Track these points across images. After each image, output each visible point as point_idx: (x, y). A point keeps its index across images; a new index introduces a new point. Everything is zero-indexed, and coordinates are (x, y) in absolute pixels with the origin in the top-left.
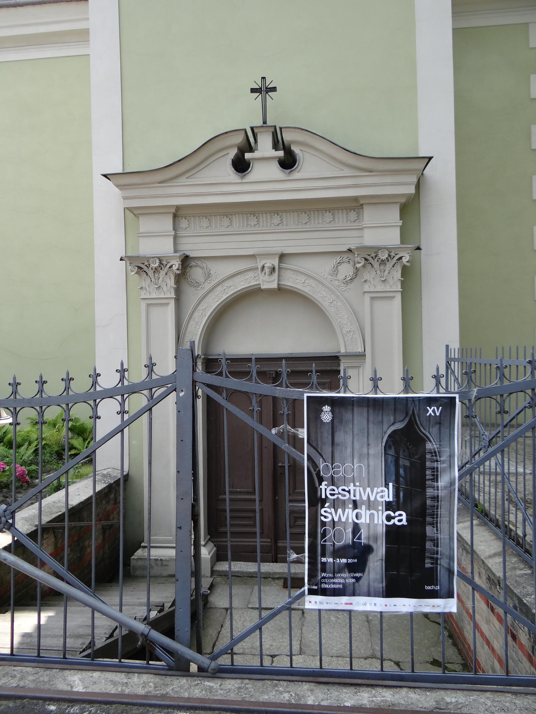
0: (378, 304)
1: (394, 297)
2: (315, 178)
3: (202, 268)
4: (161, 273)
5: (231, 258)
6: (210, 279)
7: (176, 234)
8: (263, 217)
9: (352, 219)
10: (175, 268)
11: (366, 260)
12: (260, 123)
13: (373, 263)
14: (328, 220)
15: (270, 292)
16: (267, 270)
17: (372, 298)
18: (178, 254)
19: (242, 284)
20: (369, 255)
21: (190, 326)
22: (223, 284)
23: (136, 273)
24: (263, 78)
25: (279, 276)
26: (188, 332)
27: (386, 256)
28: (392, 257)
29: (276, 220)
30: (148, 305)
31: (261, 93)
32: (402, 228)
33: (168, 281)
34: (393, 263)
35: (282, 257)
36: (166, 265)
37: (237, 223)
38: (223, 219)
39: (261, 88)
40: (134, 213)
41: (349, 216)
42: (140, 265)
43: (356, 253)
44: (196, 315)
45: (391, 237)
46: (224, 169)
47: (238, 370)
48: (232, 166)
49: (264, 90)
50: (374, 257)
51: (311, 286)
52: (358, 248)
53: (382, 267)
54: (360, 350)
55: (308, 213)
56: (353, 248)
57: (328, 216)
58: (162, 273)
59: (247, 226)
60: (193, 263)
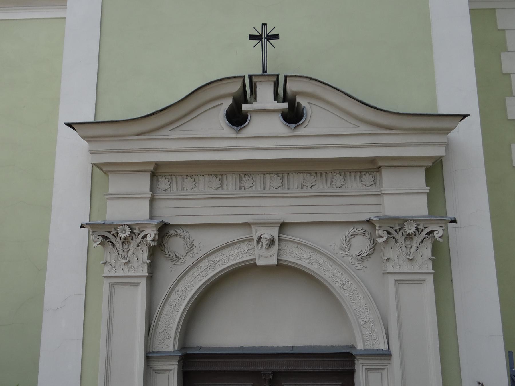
0: (404, 288)
2: (325, 134)
3: (183, 238)
4: (132, 245)
5: (220, 225)
6: (193, 251)
7: (153, 196)
8: (260, 179)
9: (368, 183)
10: (149, 238)
11: (389, 233)
12: (260, 72)
13: (397, 238)
14: (339, 184)
15: (267, 269)
16: (265, 243)
17: (397, 281)
18: (155, 222)
19: (232, 258)
20: (391, 227)
21: (164, 312)
22: (209, 258)
23: (100, 244)
24: (264, 25)
25: (279, 249)
26: (162, 319)
27: (414, 229)
28: (420, 230)
29: (276, 182)
30: (113, 285)
31: (261, 40)
32: (429, 196)
33: (140, 255)
34: (422, 238)
35: (283, 226)
36: (423, 230)
37: (229, 185)
38: (211, 180)
39: (261, 35)
40: (103, 170)
41: (363, 180)
42: (105, 234)
43: (377, 226)
44: (173, 297)
45: (417, 206)
46: (216, 120)
47: (225, 369)
48: (225, 118)
49: (264, 37)
50: (398, 231)
51: (318, 262)
53: (408, 243)
54: (383, 346)
55: (315, 174)
56: (375, 219)
57: (339, 180)
58: (133, 244)
59: (241, 189)
60: (172, 232)
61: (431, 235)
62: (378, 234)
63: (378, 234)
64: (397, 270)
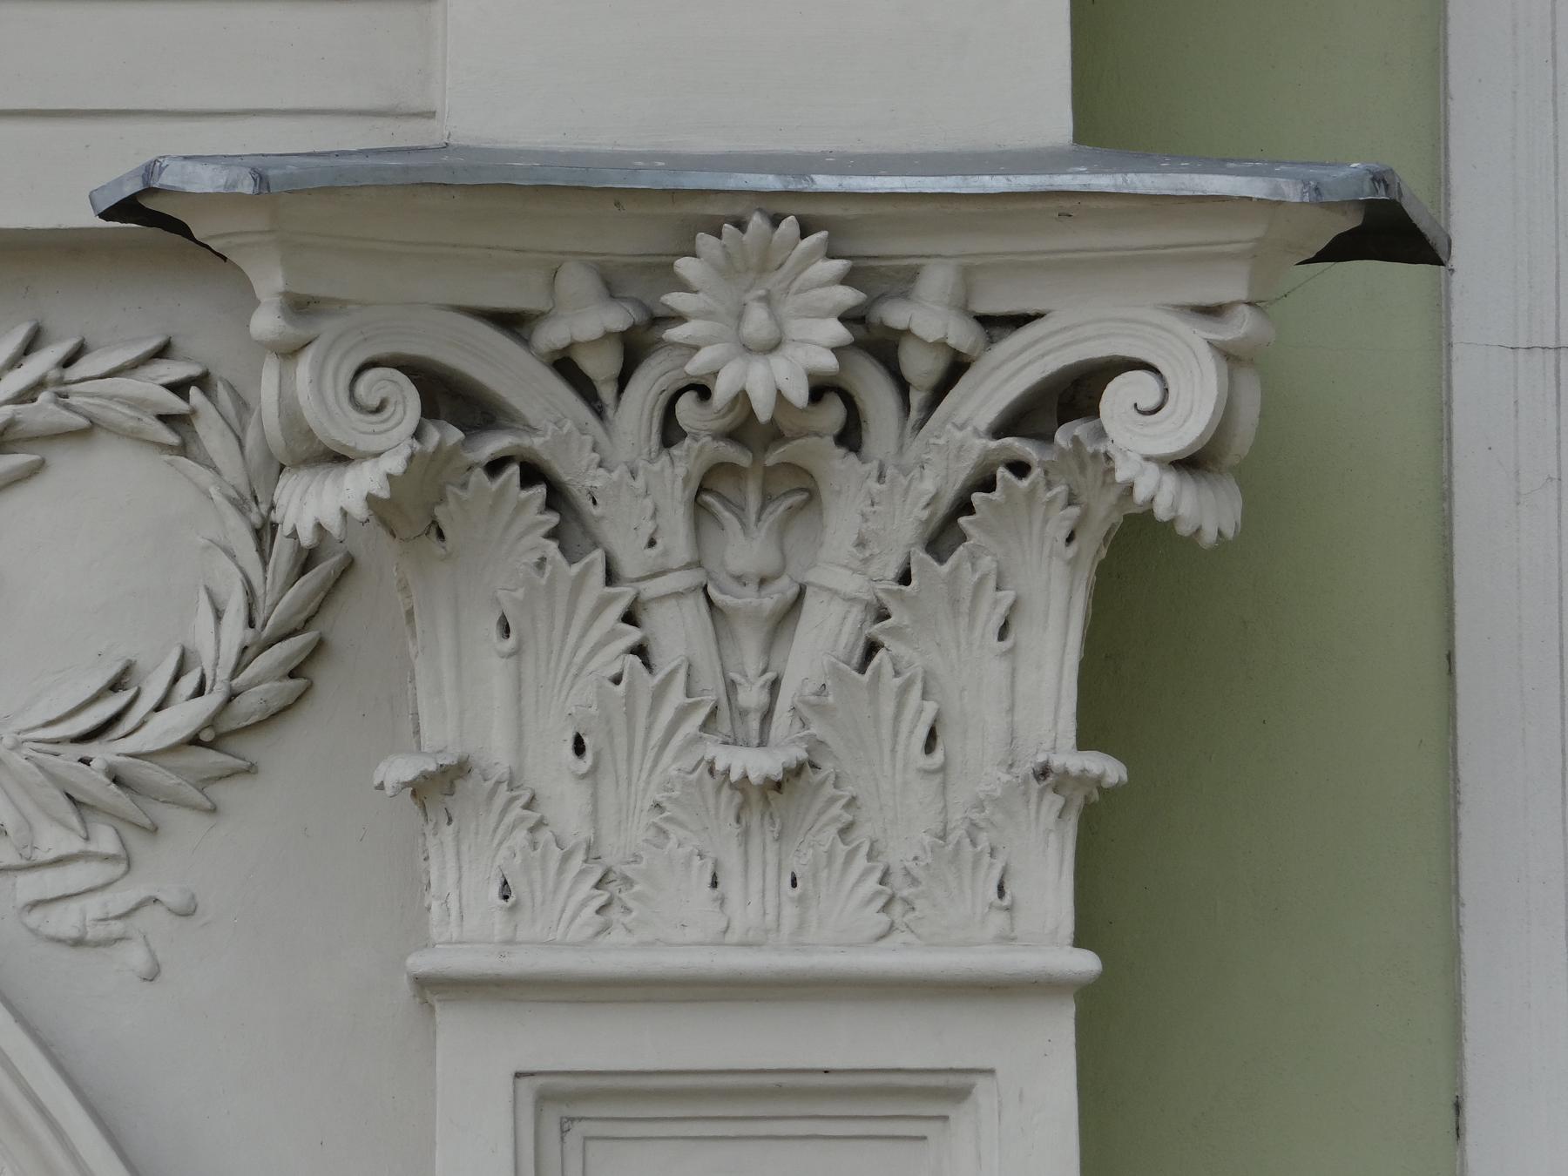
1: (948, 1090)
11: (448, 397)
13: (577, 470)
17: (559, 1100)
27: (817, 343)
28: (921, 367)
36: (957, 367)
43: (270, 281)
50: (600, 366)
52: (273, 191)
53: (744, 547)
56: (206, 180)
61: (1062, 437)
62: (291, 416)
63: (291, 416)
64: (562, 934)
